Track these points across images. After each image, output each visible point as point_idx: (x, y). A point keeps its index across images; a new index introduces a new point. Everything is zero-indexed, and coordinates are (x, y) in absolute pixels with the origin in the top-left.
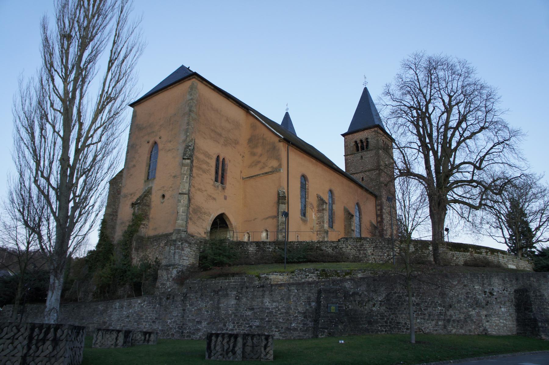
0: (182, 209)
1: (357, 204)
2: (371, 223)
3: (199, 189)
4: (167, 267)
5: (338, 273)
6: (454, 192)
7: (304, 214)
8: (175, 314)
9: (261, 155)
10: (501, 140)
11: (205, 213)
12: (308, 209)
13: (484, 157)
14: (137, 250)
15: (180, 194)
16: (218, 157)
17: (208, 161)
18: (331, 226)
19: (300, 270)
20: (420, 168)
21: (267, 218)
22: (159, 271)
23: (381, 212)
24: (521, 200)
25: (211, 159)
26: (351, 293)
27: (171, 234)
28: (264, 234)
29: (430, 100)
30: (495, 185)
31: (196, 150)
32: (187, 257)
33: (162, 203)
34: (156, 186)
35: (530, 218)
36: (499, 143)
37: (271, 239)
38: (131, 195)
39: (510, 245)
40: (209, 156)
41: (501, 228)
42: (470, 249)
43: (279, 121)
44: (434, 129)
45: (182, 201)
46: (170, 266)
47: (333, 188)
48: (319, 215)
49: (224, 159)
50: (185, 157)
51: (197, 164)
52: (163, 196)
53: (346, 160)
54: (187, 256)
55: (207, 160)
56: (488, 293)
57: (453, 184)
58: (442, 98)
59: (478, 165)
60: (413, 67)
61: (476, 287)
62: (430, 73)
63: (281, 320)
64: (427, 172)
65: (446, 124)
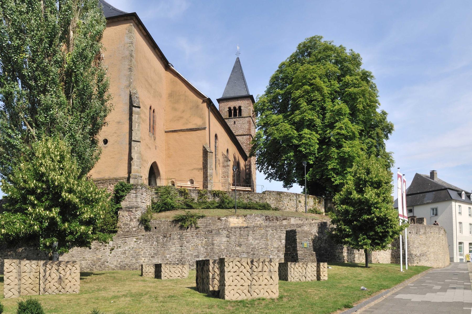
0: (136, 155)
8: (173, 249)
11: (145, 161)
48: (225, 169)
63: (262, 253)
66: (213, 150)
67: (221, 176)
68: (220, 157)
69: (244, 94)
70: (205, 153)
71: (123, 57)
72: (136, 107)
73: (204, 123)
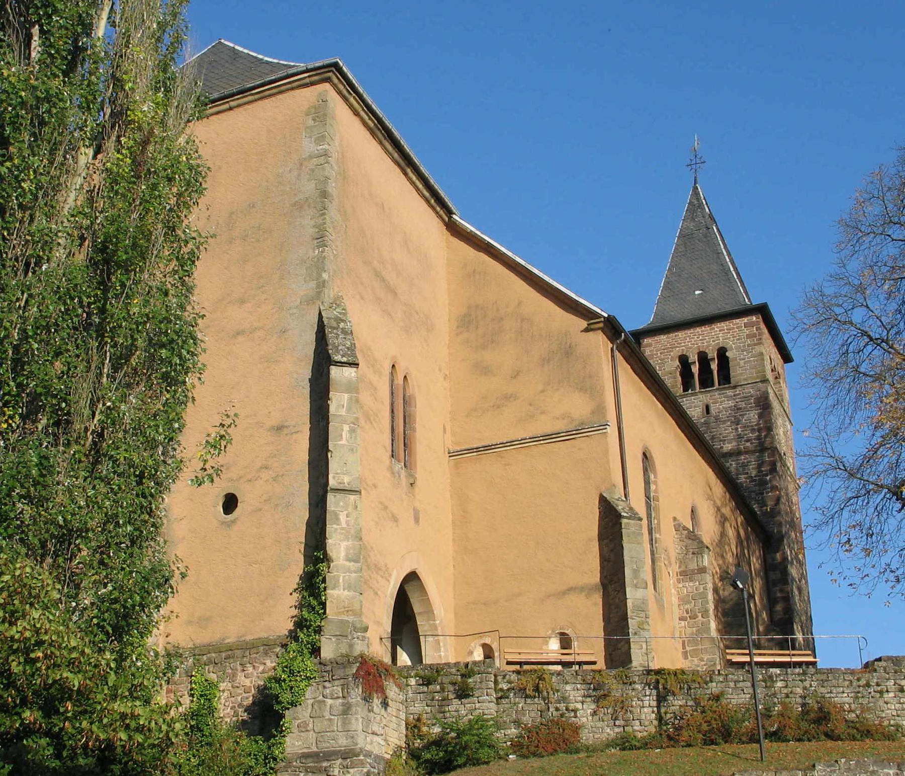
9: (516, 375)
21: (564, 593)
52: (230, 503)
66: (640, 507)
67: (677, 613)
68: (669, 539)
70: (611, 521)
71: (294, 205)
72: (342, 364)
73: (600, 409)
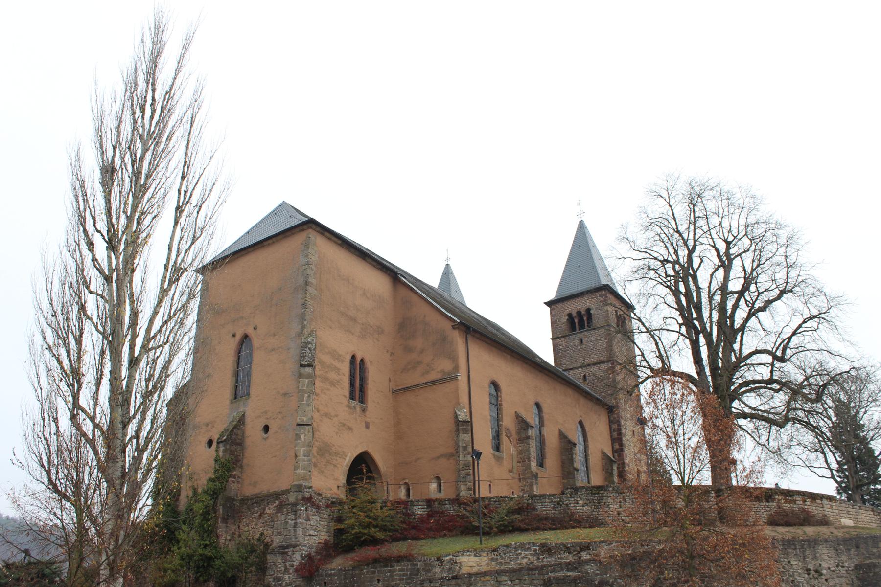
1: (581, 423)
2: (603, 453)
3: (326, 415)
4: (284, 550)
5: (568, 548)
6: (744, 403)
7: (497, 448)
9: (422, 351)
10: (815, 312)
11: (337, 454)
12: (504, 439)
13: (790, 338)
14: (225, 520)
15: (298, 425)
16: (353, 357)
17: (338, 365)
18: (541, 464)
19: (507, 546)
20: (683, 362)
21: (438, 457)
22: (269, 557)
23: (620, 434)
24: (852, 405)
25: (342, 361)
26: (596, 582)
27: (287, 492)
28: (434, 486)
29: (694, 246)
30: (810, 385)
31: (318, 349)
32: (312, 531)
33: (265, 439)
34: (255, 410)
35: (871, 434)
36: (811, 318)
37: (447, 493)
38: (207, 425)
39: (839, 480)
40: (338, 357)
41: (823, 453)
42: (777, 497)
43: (433, 280)
44: (702, 294)
45: (302, 437)
46: (287, 547)
47: (540, 400)
48: (522, 446)
49: (362, 360)
50: (304, 363)
51: (321, 372)
52: (266, 429)
53: (555, 346)
54: (315, 530)
55: (336, 363)
56: (812, 572)
57: (741, 385)
58: (714, 246)
59: (779, 353)
60: (665, 195)
61: (794, 563)
62: (692, 204)
64: (696, 368)
65: (724, 288)
69: (593, 284)
